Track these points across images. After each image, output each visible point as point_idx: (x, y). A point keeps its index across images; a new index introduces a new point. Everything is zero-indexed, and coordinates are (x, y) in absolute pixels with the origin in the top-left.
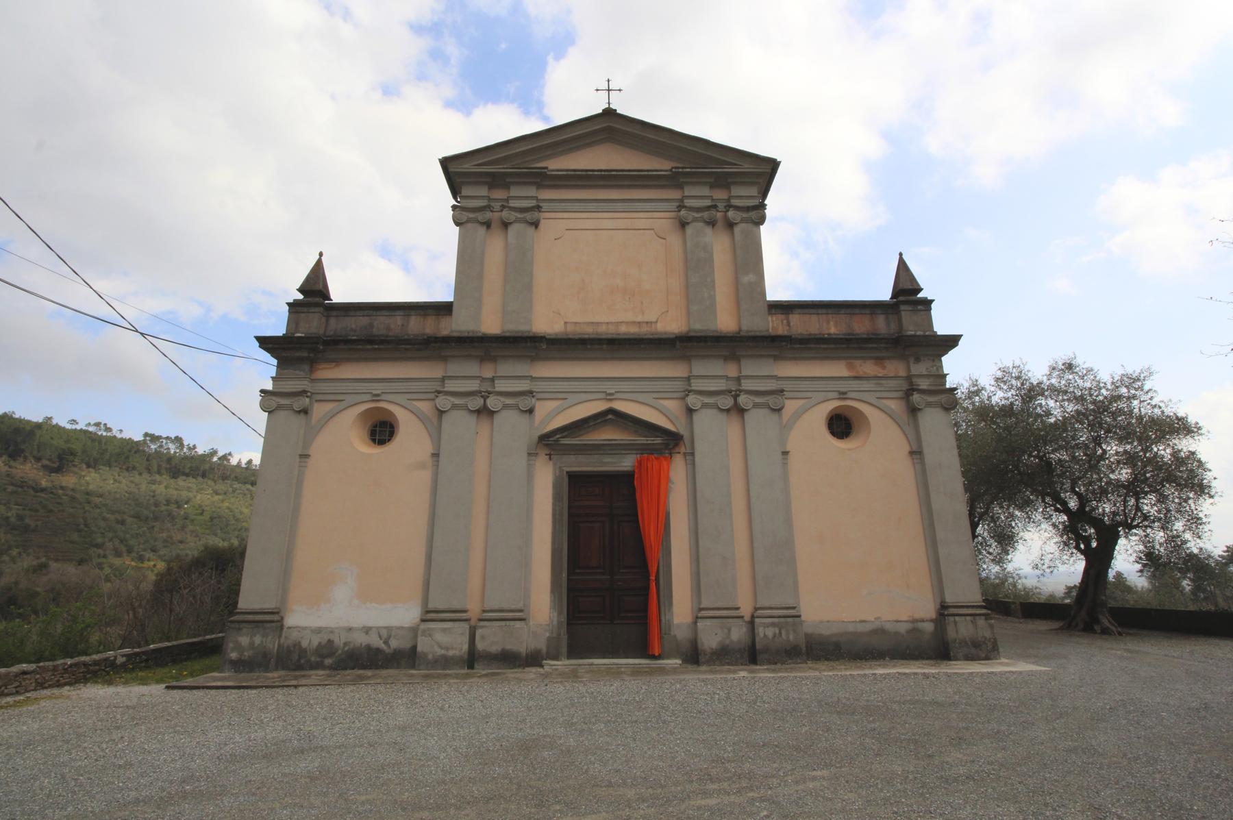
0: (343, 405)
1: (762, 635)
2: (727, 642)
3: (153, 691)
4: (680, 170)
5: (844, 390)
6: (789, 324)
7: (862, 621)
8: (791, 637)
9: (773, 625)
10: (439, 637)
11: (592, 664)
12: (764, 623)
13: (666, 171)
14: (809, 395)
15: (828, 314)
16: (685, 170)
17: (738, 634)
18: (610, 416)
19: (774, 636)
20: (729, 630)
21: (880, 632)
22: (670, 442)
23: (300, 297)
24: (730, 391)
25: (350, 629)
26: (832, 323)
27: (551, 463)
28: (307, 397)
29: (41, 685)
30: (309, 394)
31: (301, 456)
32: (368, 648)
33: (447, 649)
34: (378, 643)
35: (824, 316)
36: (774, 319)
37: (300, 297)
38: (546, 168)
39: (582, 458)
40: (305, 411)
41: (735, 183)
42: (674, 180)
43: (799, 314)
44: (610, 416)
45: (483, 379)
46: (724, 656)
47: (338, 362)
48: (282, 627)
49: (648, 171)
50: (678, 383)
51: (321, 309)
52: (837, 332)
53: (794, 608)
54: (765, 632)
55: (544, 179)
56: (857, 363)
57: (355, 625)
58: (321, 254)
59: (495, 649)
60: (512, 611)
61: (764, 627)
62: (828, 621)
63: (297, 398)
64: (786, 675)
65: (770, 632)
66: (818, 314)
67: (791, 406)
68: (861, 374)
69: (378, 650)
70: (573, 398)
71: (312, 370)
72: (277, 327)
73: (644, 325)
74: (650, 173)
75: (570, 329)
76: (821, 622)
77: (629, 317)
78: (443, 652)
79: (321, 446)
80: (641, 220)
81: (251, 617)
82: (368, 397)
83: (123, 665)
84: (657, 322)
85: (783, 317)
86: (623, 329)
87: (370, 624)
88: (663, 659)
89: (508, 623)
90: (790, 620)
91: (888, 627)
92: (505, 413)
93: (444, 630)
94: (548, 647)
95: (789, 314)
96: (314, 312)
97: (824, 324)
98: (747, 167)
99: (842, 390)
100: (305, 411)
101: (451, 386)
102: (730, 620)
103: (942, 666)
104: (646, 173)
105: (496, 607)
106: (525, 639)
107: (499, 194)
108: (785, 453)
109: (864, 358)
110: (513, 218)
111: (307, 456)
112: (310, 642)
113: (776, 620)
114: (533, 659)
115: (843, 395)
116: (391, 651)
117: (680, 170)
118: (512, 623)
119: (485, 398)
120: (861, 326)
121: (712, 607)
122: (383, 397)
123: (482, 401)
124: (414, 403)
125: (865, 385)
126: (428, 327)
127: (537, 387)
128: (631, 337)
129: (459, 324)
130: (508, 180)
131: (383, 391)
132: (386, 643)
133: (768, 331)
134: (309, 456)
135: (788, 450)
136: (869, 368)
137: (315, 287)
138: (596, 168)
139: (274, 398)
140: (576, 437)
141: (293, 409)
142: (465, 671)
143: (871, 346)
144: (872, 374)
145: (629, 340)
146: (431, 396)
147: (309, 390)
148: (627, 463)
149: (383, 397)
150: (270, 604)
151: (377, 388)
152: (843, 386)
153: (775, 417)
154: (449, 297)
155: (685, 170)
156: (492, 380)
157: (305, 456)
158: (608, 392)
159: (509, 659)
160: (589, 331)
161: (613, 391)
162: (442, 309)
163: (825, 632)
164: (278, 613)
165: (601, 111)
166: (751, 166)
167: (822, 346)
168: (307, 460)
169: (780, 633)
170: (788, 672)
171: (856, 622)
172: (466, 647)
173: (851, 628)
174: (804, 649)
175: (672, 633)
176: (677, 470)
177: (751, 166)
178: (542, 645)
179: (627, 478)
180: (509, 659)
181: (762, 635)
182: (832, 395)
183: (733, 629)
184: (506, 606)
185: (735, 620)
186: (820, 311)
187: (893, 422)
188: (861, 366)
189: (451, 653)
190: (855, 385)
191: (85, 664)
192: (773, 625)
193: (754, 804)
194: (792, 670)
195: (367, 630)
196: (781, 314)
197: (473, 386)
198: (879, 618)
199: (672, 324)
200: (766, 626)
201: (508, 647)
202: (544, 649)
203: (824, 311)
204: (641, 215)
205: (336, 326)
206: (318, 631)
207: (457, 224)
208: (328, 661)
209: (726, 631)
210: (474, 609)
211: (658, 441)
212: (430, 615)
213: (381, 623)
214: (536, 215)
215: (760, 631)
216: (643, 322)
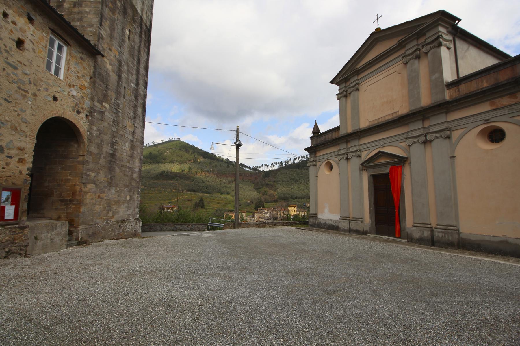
0: (322, 162)
1: (437, 235)
2: (423, 236)
3: (294, 228)
4: (400, 41)
5: (487, 118)
6: (459, 91)
7: (493, 236)
8: (450, 238)
9: (442, 232)
10: (343, 224)
11: (379, 237)
12: (438, 231)
13: (396, 44)
14: (466, 126)
15: (482, 77)
16: (402, 40)
17: (427, 234)
18: (380, 154)
19: (442, 236)
20: (423, 232)
21: (506, 242)
22: (402, 161)
23: (313, 134)
24: (423, 134)
25: (328, 220)
26: (485, 81)
27: (367, 172)
28: (448, 130)
29: (282, 225)
30: (449, 129)
31: (451, 157)
32: (332, 224)
33: (344, 227)
34: (333, 224)
35: (480, 79)
36: (451, 91)
37: (313, 134)
38: (357, 68)
39: (375, 170)
40: (448, 137)
41: (427, 31)
42: (401, 45)
43: (465, 83)
44: (380, 154)
45: (448, 122)
46: (421, 241)
47: (319, 151)
48: (317, 218)
49: (389, 49)
50: (406, 135)
51: (316, 137)
52: (488, 85)
53: (316, 215)
54: (438, 235)
55: (358, 72)
56: (497, 101)
57: (329, 219)
58: (316, 121)
59: (354, 228)
60: (451, 226)
61: (438, 233)
62: (474, 234)
63: (420, 138)
64: (460, 255)
65: (440, 235)
66: (476, 79)
67: (455, 135)
68: (499, 106)
69: (334, 226)
70: (371, 149)
71: (315, 154)
72: (309, 145)
73: (394, 114)
74: (392, 48)
75: (370, 124)
76: (471, 234)
77: (390, 112)
78: (344, 228)
79: (460, 151)
80: (392, 70)
81: (312, 215)
82: (326, 159)
83: (298, 224)
84: (398, 111)
85: (456, 88)
86: (387, 118)
87: (332, 219)
88: (401, 239)
89: (357, 222)
90: (449, 231)
91: (510, 240)
92: (436, 141)
93: (344, 222)
94: (369, 230)
95: (459, 85)
96: (508, 67)
97: (480, 83)
98: (429, 22)
99: (485, 119)
100: (448, 137)
101: (411, 135)
102: (424, 228)
103: (511, 261)
104: (389, 50)
105: (355, 217)
106: (361, 227)
107: (421, 40)
108: (453, 157)
109: (502, 97)
110: (351, 91)
111: (454, 157)
112: (322, 222)
113: (443, 230)
114: (365, 233)
115: (487, 121)
116: (336, 226)
117: (400, 41)
118: (358, 222)
119: (426, 136)
120: (485, 84)
121: (418, 222)
122: (329, 158)
123: (424, 138)
124: (400, 144)
125: (501, 112)
126: (334, 135)
127: (449, 126)
128: (391, 120)
129: (342, 132)
130: (424, 32)
131: (491, 117)
132: (335, 224)
133: (445, 99)
134: (455, 156)
135: (455, 155)
136: (505, 101)
137: (316, 130)
138: (372, 59)
139: (411, 140)
140: (373, 162)
141: (443, 137)
142: (349, 233)
143: (500, 90)
144: (507, 104)
145: (383, 124)
146: (404, 140)
147: (423, 133)
148: (387, 170)
149: (329, 158)
150: (314, 213)
151: (327, 156)
152: (486, 117)
153: (447, 141)
154: (338, 124)
155: (402, 40)
156: (428, 127)
157: (317, 177)
158: (381, 144)
159: (357, 232)
160: (381, 121)
161: (383, 144)
162: (337, 129)
163: (473, 238)
164: (316, 215)
165: (370, 35)
166: (431, 20)
167: (469, 100)
168: (455, 159)
169: (445, 236)
170: (484, 257)
171: (490, 236)
172: (348, 227)
173: (487, 239)
174: (456, 244)
175: (406, 231)
176: (406, 171)
177: (431, 20)
178: (368, 229)
179: (386, 175)
180: (357, 232)
181: (437, 235)
182: (480, 123)
183: (425, 232)
184: (357, 217)
185: (426, 228)
186: (477, 77)
187: (461, 140)
188: (499, 101)
189: (345, 228)
190: (495, 113)
191: (290, 222)
192: (442, 232)
193: (178, 208)
194: (450, 252)
195: (331, 220)
196: (455, 87)
197: (421, 132)
198: (505, 236)
199: (403, 109)
200: (438, 232)
201: (357, 228)
202: (368, 229)
203: (479, 76)
204: (391, 67)
205: (322, 139)
206: (323, 219)
207: (338, 100)
208: (326, 227)
209: (422, 232)
210: (434, 225)
211: (396, 160)
212: (342, 218)
213: (334, 219)
214: (357, 86)
215: (436, 234)
216: (394, 113)
